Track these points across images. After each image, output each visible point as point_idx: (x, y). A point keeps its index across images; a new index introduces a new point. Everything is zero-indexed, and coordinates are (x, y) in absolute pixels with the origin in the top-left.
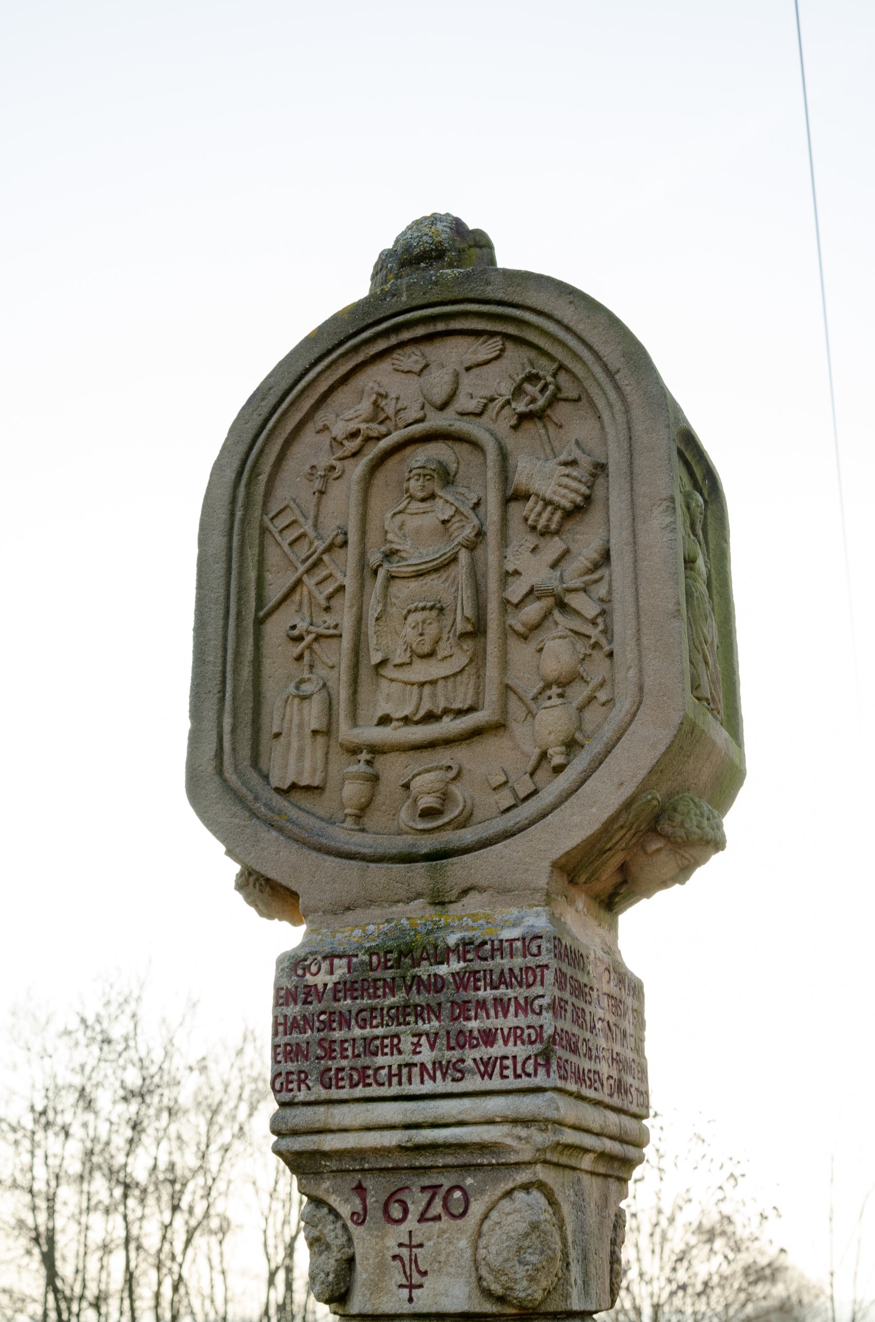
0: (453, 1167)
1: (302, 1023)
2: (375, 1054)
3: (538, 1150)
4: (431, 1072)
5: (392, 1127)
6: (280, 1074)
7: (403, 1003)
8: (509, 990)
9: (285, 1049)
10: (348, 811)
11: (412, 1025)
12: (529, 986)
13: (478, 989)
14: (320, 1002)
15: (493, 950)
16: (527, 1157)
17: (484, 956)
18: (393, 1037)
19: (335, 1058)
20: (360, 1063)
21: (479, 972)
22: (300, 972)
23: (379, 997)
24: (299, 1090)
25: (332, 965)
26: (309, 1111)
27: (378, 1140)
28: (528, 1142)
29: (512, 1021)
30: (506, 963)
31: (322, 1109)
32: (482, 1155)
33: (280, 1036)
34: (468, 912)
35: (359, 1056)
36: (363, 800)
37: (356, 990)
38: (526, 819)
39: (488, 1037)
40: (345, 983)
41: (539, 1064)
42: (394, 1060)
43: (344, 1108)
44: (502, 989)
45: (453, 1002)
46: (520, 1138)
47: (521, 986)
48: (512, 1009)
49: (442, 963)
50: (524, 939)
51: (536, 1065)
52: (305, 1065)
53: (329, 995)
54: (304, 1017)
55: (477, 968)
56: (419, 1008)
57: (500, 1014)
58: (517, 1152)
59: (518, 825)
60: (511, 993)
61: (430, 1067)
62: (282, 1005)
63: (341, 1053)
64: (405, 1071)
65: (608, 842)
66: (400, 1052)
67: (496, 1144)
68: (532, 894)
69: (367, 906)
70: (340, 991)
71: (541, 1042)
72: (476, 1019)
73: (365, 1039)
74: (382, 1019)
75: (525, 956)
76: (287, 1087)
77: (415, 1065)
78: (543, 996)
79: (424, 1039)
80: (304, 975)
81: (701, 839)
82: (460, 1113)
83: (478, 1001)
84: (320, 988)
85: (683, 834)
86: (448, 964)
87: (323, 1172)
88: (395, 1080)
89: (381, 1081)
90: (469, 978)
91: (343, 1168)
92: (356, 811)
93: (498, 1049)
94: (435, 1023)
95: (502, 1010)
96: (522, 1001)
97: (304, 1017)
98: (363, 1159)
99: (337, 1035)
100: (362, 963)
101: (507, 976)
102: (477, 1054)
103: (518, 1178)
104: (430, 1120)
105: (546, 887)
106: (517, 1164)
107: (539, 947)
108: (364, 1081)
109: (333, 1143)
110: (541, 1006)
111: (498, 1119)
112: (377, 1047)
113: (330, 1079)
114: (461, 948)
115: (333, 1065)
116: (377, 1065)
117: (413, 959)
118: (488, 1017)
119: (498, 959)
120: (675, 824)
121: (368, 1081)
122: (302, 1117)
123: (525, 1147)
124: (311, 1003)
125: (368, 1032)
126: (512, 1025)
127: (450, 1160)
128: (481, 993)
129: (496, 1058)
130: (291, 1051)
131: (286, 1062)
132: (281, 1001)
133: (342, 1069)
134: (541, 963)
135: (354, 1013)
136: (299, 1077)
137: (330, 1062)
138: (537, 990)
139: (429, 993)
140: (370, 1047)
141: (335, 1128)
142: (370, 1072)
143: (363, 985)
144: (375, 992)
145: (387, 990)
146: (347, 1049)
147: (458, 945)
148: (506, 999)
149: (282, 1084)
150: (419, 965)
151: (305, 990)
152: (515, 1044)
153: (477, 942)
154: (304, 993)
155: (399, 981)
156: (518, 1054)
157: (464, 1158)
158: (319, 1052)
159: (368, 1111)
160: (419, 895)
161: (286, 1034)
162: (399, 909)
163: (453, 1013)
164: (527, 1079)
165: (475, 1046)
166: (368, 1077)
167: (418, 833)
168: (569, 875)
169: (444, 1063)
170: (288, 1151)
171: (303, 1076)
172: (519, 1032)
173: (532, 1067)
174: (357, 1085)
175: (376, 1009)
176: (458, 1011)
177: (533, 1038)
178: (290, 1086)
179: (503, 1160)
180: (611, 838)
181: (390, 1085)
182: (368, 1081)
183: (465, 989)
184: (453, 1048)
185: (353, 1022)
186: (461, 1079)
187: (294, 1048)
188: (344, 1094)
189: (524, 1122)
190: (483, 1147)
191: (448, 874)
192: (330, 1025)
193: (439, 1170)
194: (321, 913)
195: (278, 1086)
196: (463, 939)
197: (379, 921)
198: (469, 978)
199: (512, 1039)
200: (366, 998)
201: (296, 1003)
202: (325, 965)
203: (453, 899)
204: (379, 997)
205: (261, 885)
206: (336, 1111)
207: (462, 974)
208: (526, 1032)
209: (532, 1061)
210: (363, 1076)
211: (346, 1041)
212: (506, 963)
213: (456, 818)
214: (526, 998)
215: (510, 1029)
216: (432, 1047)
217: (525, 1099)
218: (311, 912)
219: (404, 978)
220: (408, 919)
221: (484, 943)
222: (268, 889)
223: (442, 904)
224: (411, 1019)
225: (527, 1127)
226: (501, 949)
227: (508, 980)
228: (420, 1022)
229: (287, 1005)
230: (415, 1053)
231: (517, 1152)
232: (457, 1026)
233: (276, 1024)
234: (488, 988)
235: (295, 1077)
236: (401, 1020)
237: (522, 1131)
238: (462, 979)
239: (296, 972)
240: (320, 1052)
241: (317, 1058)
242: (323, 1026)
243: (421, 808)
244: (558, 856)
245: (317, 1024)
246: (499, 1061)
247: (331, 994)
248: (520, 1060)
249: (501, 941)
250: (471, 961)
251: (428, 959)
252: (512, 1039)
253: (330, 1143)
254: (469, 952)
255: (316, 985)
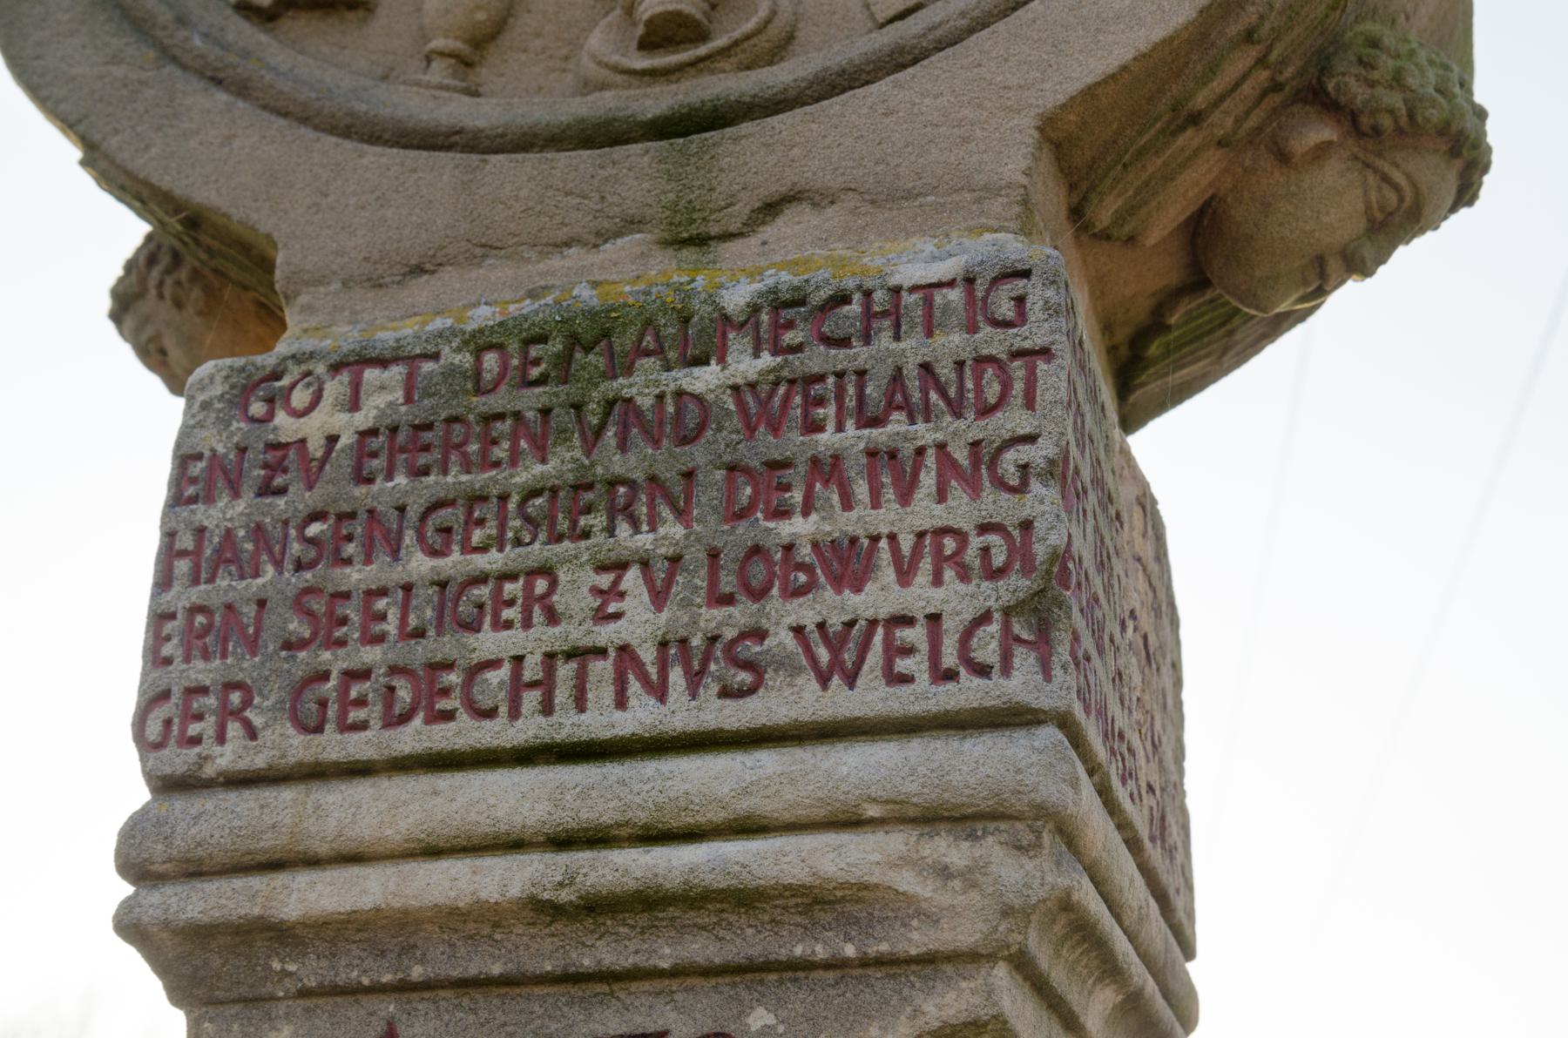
0: (707, 972)
1: (249, 546)
2: (473, 627)
3: (1007, 912)
4: (653, 671)
5: (515, 844)
6: (165, 695)
7: (570, 477)
8: (920, 427)
9: (190, 621)
10: (439, 43)
11: (598, 538)
12: (986, 411)
13: (818, 427)
14: (310, 488)
15: (869, 315)
16: (965, 933)
17: (840, 333)
18: (533, 573)
19: (341, 643)
20: (420, 652)
21: (821, 378)
22: (257, 408)
23: (497, 464)
24: (221, 739)
25: (356, 386)
26: (246, 803)
27: (462, 884)
28: (974, 885)
29: (926, 511)
30: (913, 349)
31: (287, 795)
32: (810, 931)
33: (177, 587)
34: (778, 258)
35: (420, 633)
36: (481, 16)
37: (426, 448)
38: (963, 14)
39: (844, 562)
40: (394, 430)
41: (1018, 640)
42: (534, 641)
43: (361, 791)
44: (898, 423)
45: (732, 468)
46: (944, 873)
47: (958, 415)
48: (928, 480)
49: (701, 361)
50: (970, 281)
51: (1009, 642)
52: (246, 667)
53: (342, 463)
54: (258, 532)
55: (815, 367)
56: (622, 490)
57: (889, 494)
58: (932, 919)
59: (939, 32)
60: (925, 433)
61: (648, 655)
62: (193, 500)
63: (364, 629)
64: (565, 671)
65: (1203, 81)
66: (552, 617)
67: (861, 892)
68: (978, 201)
69: (474, 260)
70: (374, 455)
71: (1027, 570)
72: (806, 514)
73: (443, 585)
74: (502, 527)
75: (972, 328)
76: (183, 731)
77: (601, 652)
78: (1031, 439)
79: (632, 579)
80: (270, 416)
81: (1443, 130)
82: (746, 792)
83: (815, 461)
84: (316, 447)
85: (1400, 105)
86: (722, 360)
87: (273, 998)
88: (531, 699)
89: (486, 703)
90: (787, 399)
91: (341, 979)
92: (458, 45)
93: (879, 596)
94: (673, 530)
95: (896, 482)
96: (961, 455)
97: (258, 532)
98: (407, 950)
99: (356, 576)
100: (452, 372)
101: (913, 385)
102: (806, 612)
103: (929, 1007)
104: (642, 817)
105: (1024, 180)
106: (929, 960)
107: (1020, 300)
108: (431, 706)
109: (312, 896)
110: (1024, 468)
111: (873, 811)
112: (481, 606)
113: (323, 704)
114: (765, 317)
115: (336, 661)
116: (476, 658)
117: (611, 354)
118: (847, 505)
119: (885, 341)
120: (1376, 75)
121: (443, 704)
122: (222, 820)
123: (961, 899)
124: (281, 491)
125: (454, 563)
126: (927, 524)
127: (700, 949)
128: (827, 439)
129: (873, 623)
130: (207, 629)
131: (187, 659)
132: (190, 491)
133: (364, 674)
134: (1027, 345)
135: (413, 513)
136: (224, 701)
137: (326, 655)
138: (1015, 420)
139: (656, 443)
140: (456, 605)
141: (323, 849)
142: (453, 678)
143: (448, 433)
144: (484, 453)
145: (523, 444)
146: (383, 617)
147: (755, 309)
148: (908, 450)
149: (168, 723)
150: (629, 371)
151: (270, 457)
152: (937, 580)
153: (818, 298)
154: (266, 466)
155: (563, 417)
156: (947, 608)
157: (748, 941)
158: (293, 626)
159: (436, 793)
160: (632, 224)
161: (195, 581)
162: (568, 263)
163: (731, 497)
164: (977, 681)
165: (800, 592)
166: (446, 692)
167: (634, 81)
168: (1072, 187)
169: (696, 641)
170: (166, 924)
171: (236, 698)
172: (950, 544)
173: (994, 645)
174: (405, 718)
175: (484, 499)
176: (748, 491)
177: (999, 559)
178: (194, 729)
179: (884, 947)
180: (1213, 69)
181: (515, 714)
182: (443, 704)
183: (775, 430)
184: (728, 600)
185: (409, 537)
186: (751, 690)
187: (217, 618)
188: (359, 746)
189: (964, 818)
190: (816, 901)
191: (724, 163)
192: (337, 551)
193: (658, 984)
194: (336, 286)
195: (154, 730)
196: (774, 291)
197: (508, 295)
198: (787, 399)
199: (926, 565)
200: (454, 470)
201: (236, 495)
202: (335, 388)
203: (733, 228)
204: (497, 464)
205: (178, 283)
206: (331, 799)
207: (764, 389)
208: (976, 542)
209: (994, 628)
210: (430, 692)
211: (383, 592)
212: (913, 349)
213: (748, 37)
214: (975, 444)
215: (921, 535)
216: (659, 597)
217: (968, 744)
218: (306, 283)
219: (578, 407)
220: (595, 284)
221: (843, 299)
222: (197, 293)
223: (701, 241)
224: (597, 521)
225: (972, 836)
226: (895, 315)
227: (916, 396)
228: (623, 529)
229: (210, 499)
230: (602, 617)
231: (932, 919)
232: (744, 533)
233: (169, 553)
234: (850, 424)
235: (211, 701)
236: (563, 525)
237: (950, 850)
238: (764, 404)
239: (245, 408)
240: (297, 627)
241: (288, 645)
242: (312, 554)
243: (646, 17)
244: (1061, 98)
245: (296, 548)
246: (880, 631)
247: (347, 464)
248: (951, 629)
249: (896, 291)
250: (797, 349)
251: (659, 352)
252: (926, 565)
253: (303, 896)
254: (790, 325)
255: (303, 441)
